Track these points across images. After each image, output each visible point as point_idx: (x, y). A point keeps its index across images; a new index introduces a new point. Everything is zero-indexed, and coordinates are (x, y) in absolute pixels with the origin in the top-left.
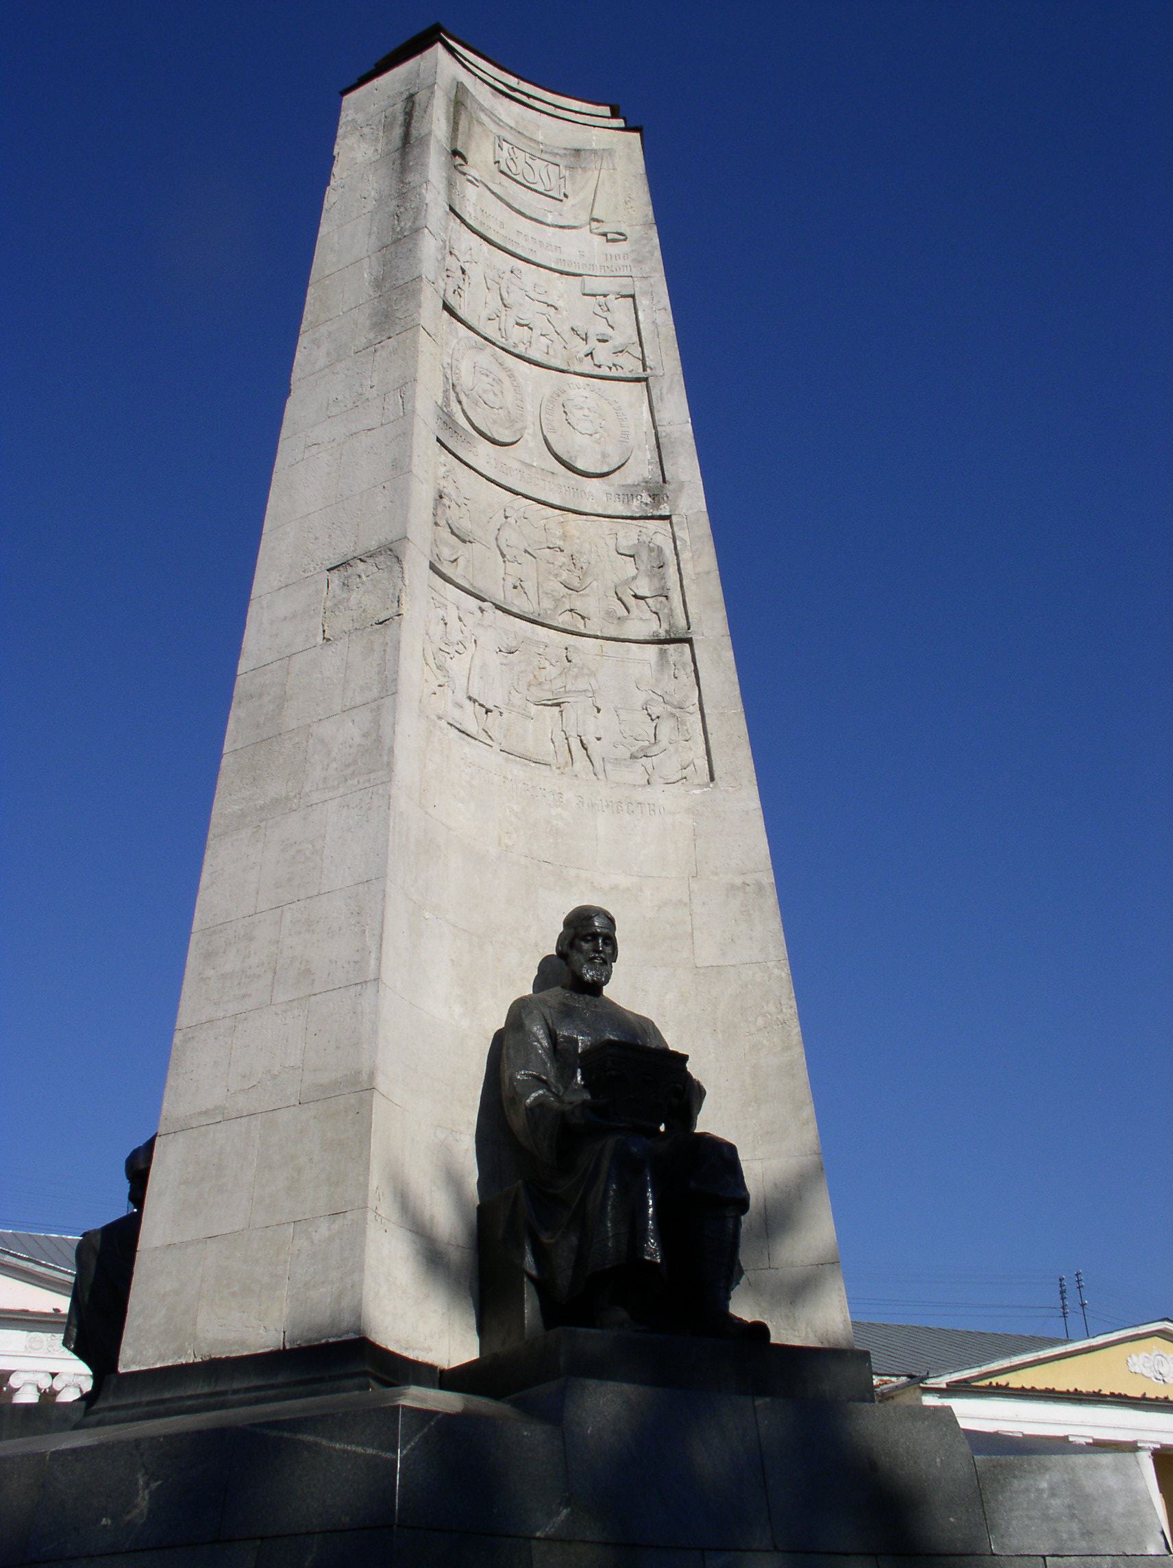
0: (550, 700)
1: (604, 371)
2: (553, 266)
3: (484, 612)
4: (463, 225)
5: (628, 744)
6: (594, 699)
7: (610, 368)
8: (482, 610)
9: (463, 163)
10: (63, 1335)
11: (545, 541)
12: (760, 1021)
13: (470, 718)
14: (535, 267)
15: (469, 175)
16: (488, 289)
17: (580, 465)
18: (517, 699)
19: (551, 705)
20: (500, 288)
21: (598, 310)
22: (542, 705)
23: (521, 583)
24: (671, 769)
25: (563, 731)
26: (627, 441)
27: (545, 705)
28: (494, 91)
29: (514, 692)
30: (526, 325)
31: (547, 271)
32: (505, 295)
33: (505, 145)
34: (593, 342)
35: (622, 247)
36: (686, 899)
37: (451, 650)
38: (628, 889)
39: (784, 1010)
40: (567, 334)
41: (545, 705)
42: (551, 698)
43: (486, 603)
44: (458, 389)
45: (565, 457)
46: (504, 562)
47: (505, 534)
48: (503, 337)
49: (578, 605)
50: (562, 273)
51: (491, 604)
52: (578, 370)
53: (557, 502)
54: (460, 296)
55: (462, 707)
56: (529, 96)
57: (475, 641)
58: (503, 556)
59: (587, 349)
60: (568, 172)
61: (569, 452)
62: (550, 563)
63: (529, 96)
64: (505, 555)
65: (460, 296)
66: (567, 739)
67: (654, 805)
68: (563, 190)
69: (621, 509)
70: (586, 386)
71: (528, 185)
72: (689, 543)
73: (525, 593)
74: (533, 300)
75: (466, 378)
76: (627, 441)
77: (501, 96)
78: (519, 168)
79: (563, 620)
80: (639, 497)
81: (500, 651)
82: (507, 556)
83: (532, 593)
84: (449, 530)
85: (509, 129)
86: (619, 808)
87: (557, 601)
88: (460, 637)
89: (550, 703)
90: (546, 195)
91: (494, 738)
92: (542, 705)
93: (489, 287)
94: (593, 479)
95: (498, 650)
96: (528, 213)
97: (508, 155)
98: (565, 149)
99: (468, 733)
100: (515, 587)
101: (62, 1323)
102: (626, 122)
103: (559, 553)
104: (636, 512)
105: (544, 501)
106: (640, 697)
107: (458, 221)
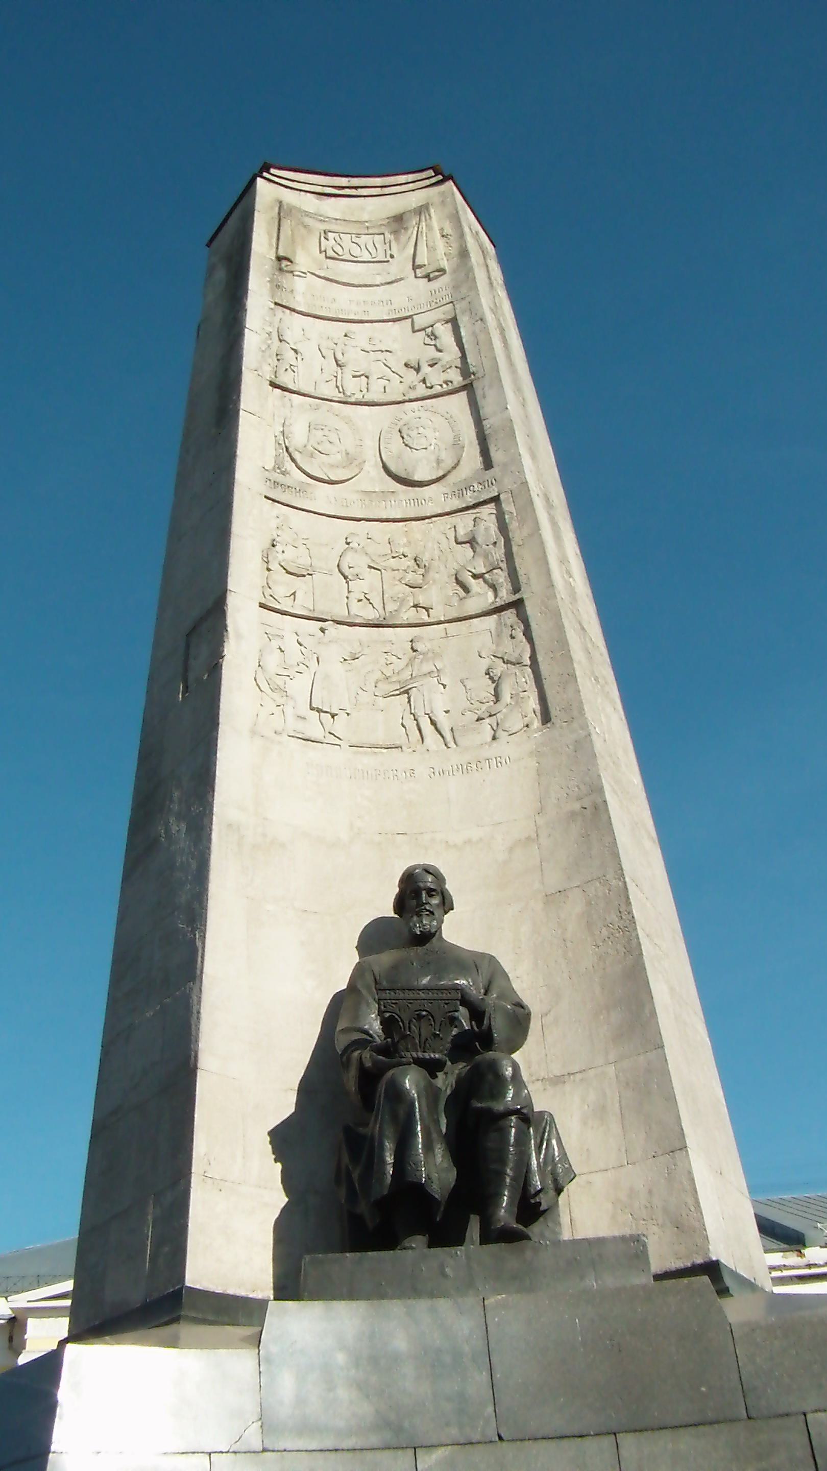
0: (397, 690)
1: (438, 389)
2: (386, 318)
3: (326, 631)
4: (293, 313)
5: (475, 709)
6: (438, 678)
7: (441, 385)
8: (323, 630)
9: (289, 263)
10: (67, 1319)
11: (390, 552)
12: (605, 932)
13: (314, 727)
14: (370, 324)
15: (296, 271)
16: (323, 357)
17: (417, 477)
18: (365, 698)
19: (398, 695)
20: (373, 351)
21: (428, 341)
22: (391, 696)
23: (366, 596)
24: (516, 723)
25: (411, 713)
26: (459, 442)
27: (393, 695)
28: (318, 196)
29: (360, 692)
30: (362, 375)
31: (380, 323)
32: (339, 356)
33: (330, 235)
34: (426, 369)
35: (445, 280)
36: (534, 835)
37: (292, 673)
38: (481, 839)
39: (624, 917)
40: (403, 371)
41: (393, 695)
42: (399, 687)
43: (327, 623)
44: (290, 450)
45: (403, 474)
46: (347, 582)
47: (348, 559)
48: (340, 392)
49: (422, 600)
50: (394, 320)
51: (331, 622)
52: (412, 396)
53: (399, 516)
54: (294, 372)
55: (305, 719)
56: (356, 188)
57: (318, 658)
58: (345, 577)
59: (420, 376)
60: (392, 236)
61: (406, 470)
62: (394, 570)
63: (356, 188)
64: (347, 576)
65: (294, 372)
66: (415, 720)
67: (500, 757)
68: (389, 252)
69: (457, 504)
70: (420, 408)
71: (356, 259)
72: (515, 514)
73: (370, 603)
74: (368, 352)
75: (299, 437)
76: (459, 442)
77: (325, 197)
78: (346, 250)
79: (409, 615)
80: (472, 488)
81: (345, 660)
82: (349, 577)
83: (377, 602)
84: (284, 571)
85: (334, 221)
86: (469, 768)
87: (403, 601)
88: (300, 658)
89: (398, 692)
90: (373, 262)
91: (341, 738)
92: (391, 696)
93: (324, 355)
94: (432, 486)
95: (342, 660)
96: (356, 283)
97: (334, 242)
98: (388, 218)
99: (312, 739)
100: (360, 600)
101: (65, 1308)
102: (443, 176)
103: (404, 559)
104: (471, 502)
105: (387, 519)
106: (485, 664)
107: (288, 311)
